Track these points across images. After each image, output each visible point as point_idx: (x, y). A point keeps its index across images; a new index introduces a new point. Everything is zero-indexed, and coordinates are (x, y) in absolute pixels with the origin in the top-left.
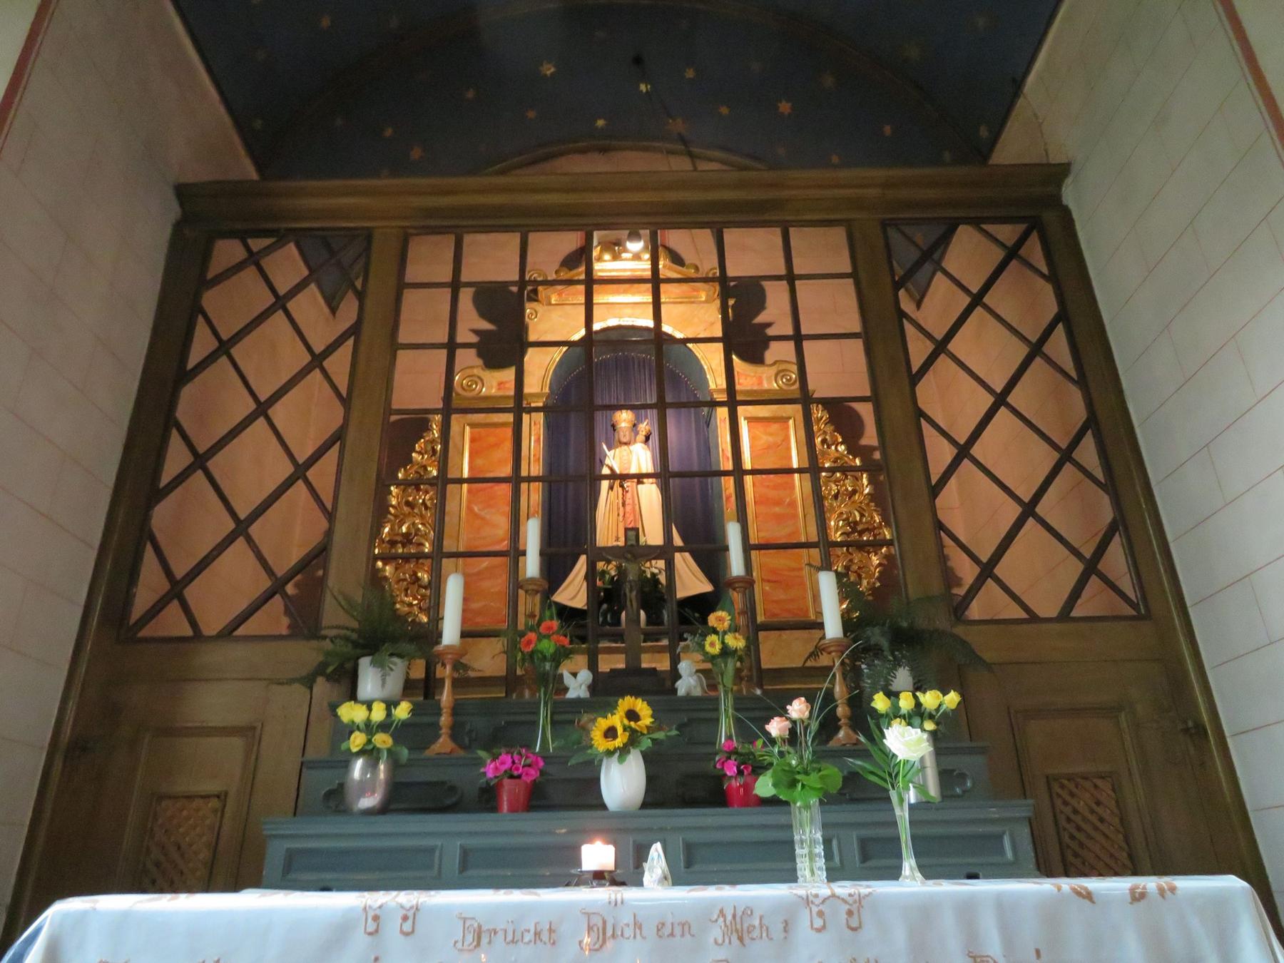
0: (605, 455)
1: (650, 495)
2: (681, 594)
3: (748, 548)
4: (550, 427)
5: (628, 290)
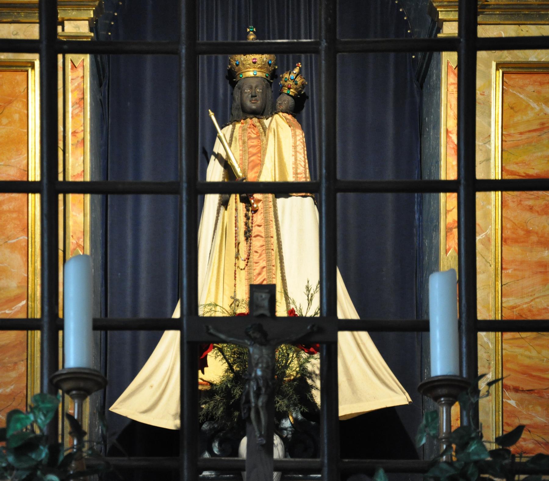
0: (215, 134)
1: (299, 221)
2: (347, 407)
3: (469, 326)
4: (99, 75)
5: (259, 102)
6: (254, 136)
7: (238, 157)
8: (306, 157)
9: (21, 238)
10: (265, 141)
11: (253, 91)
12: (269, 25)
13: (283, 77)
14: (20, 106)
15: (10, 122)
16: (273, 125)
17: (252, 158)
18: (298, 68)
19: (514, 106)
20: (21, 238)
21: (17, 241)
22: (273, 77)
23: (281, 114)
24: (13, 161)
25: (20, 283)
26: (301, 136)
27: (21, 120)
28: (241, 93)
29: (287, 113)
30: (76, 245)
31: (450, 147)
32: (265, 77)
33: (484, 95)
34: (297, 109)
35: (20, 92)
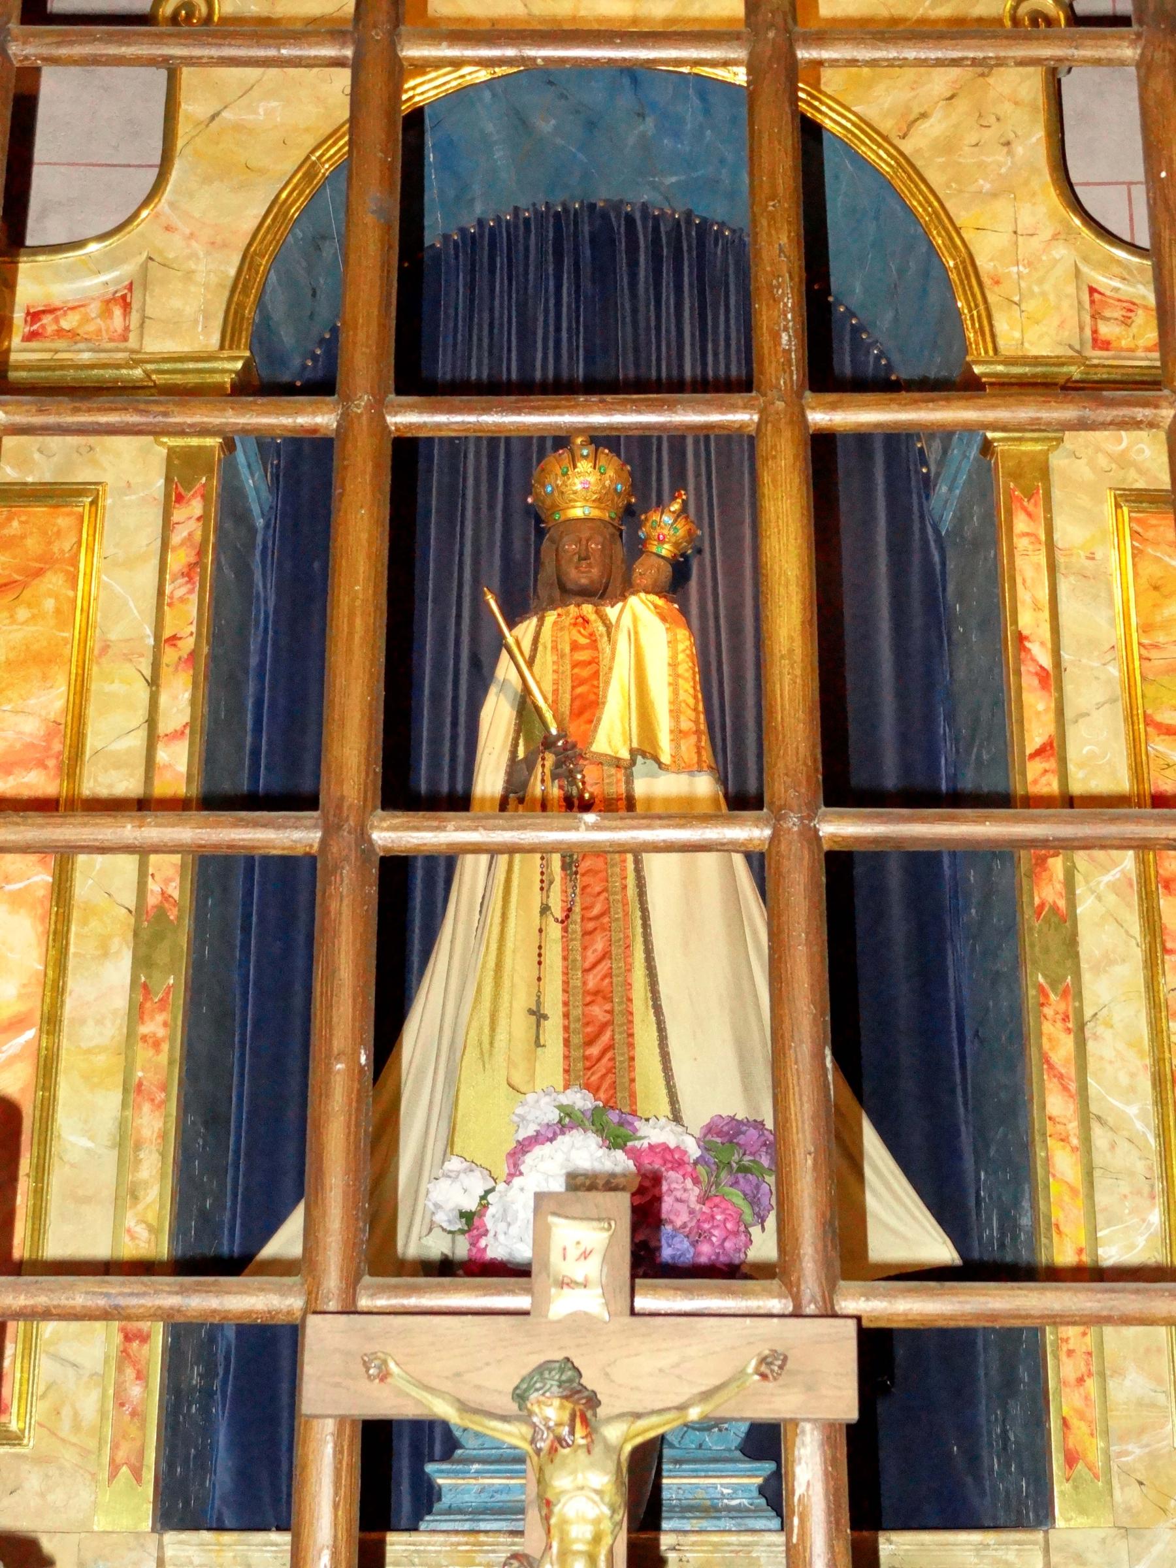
6: (583, 641)
7: (548, 687)
8: (698, 688)
9: (37, 879)
10: (608, 650)
11: (584, 548)
12: (716, 605)
13: (646, 519)
14: (60, 582)
15: (34, 617)
16: (626, 622)
17: (579, 690)
18: (679, 501)
19: (1159, 583)
20: (37, 879)
21: (26, 887)
22: (629, 517)
23: (642, 595)
24: (32, 701)
25: (24, 986)
26: (687, 643)
27: (58, 611)
28: (557, 550)
29: (657, 594)
30: (160, 898)
31: (1029, 672)
32: (607, 519)
33: (1093, 559)
34: (677, 581)
35: (62, 551)
